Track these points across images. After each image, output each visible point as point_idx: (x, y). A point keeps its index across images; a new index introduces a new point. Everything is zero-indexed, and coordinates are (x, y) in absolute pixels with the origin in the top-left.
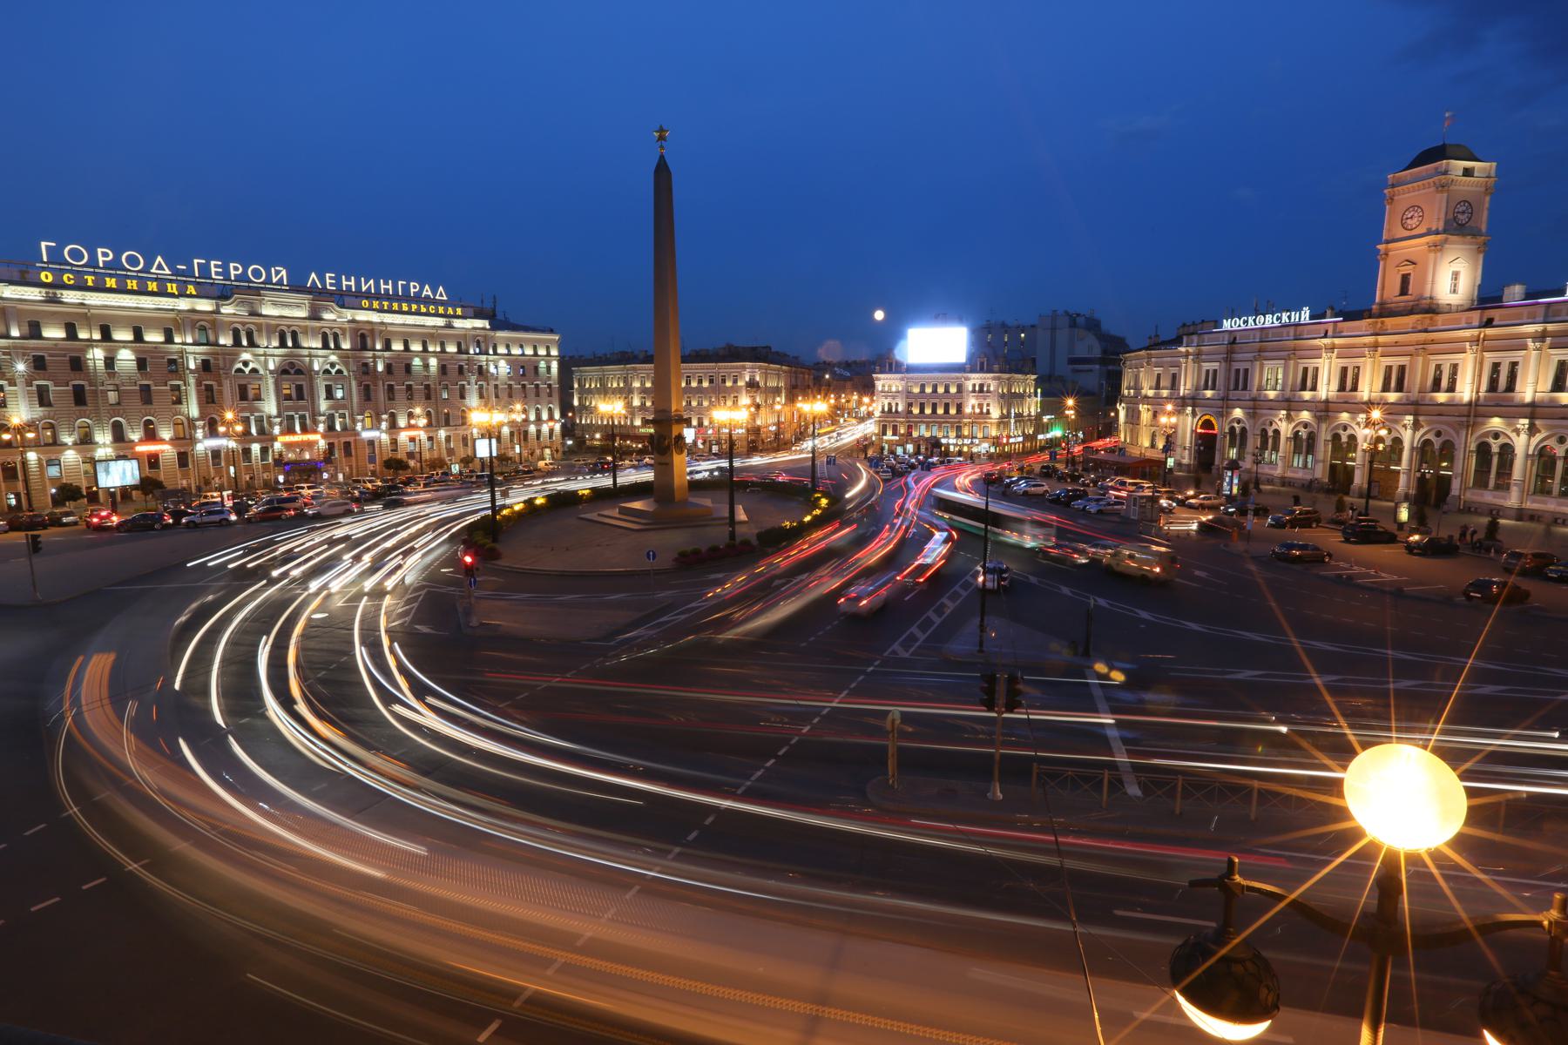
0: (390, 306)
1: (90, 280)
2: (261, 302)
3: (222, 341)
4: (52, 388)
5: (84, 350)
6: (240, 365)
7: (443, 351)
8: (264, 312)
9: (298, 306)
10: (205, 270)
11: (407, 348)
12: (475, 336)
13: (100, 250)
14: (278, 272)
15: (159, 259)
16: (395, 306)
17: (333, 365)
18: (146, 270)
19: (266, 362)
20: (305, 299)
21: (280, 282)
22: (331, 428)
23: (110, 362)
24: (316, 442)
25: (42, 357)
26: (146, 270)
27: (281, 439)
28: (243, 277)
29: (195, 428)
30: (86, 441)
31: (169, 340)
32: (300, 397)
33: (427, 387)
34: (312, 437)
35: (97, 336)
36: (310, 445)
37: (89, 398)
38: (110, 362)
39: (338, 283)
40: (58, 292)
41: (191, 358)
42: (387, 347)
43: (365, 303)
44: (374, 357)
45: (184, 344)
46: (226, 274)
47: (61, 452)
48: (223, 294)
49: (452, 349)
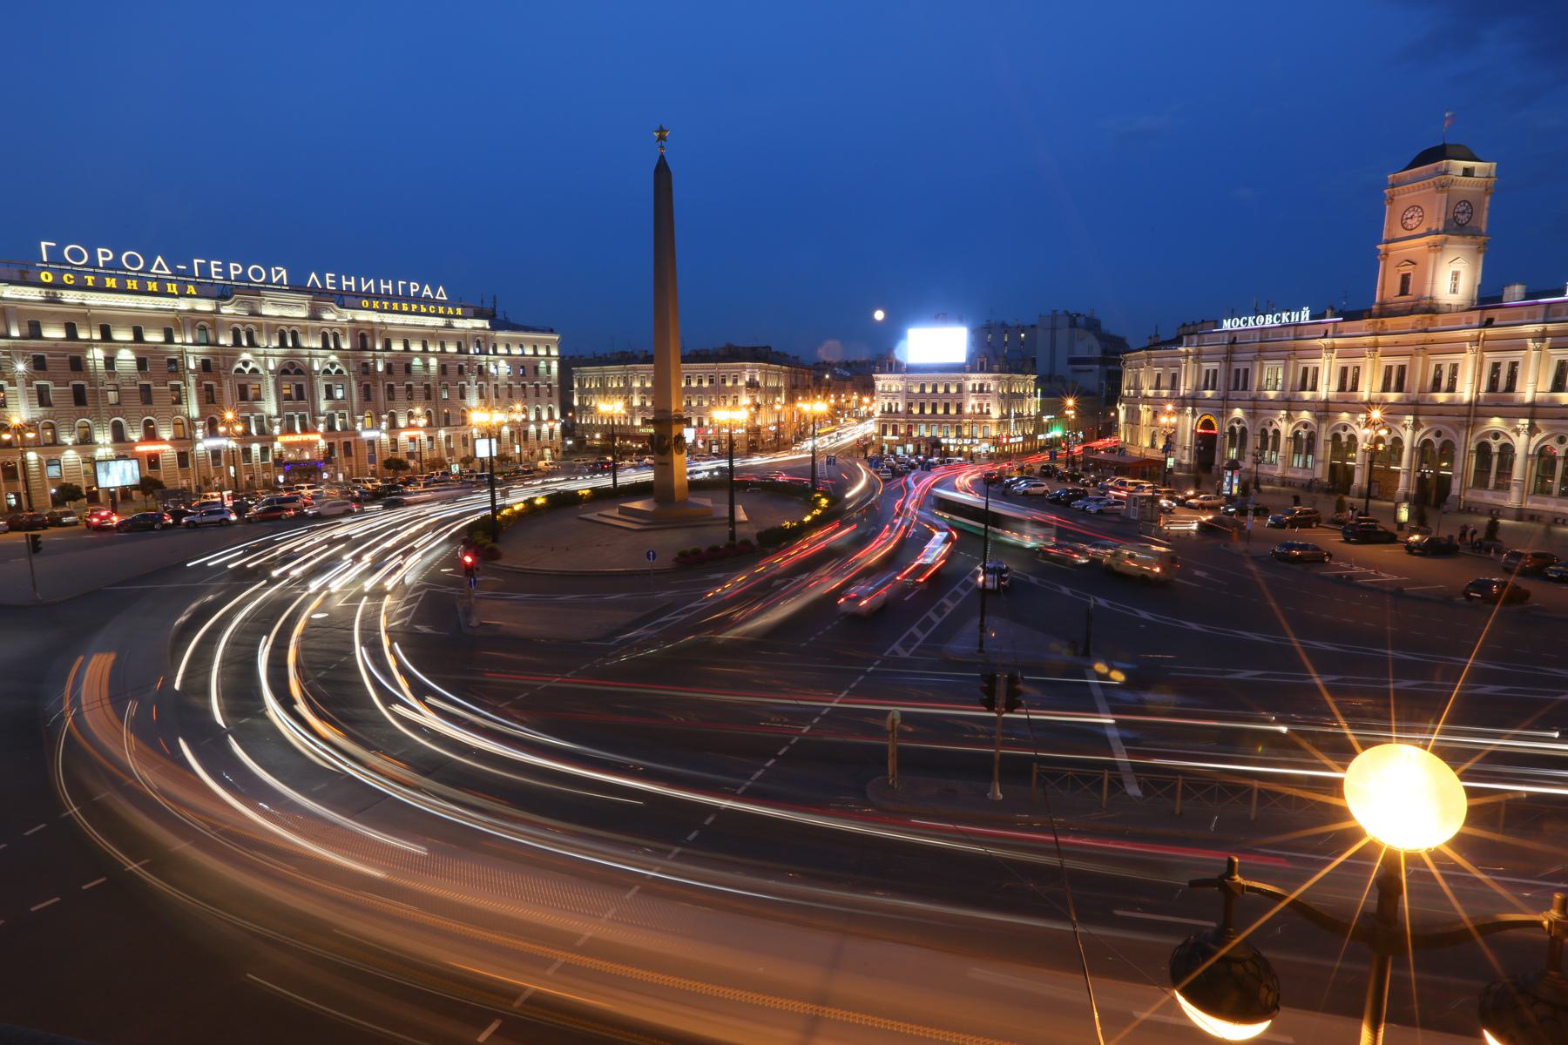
0: (390, 306)
1: (90, 280)
2: (261, 302)
3: (222, 341)
4: (52, 388)
5: (84, 350)
6: (240, 365)
7: (443, 351)
8: (264, 312)
9: (298, 306)
10: (205, 270)
11: (407, 348)
12: (475, 336)
13: (100, 250)
14: (278, 272)
15: (159, 259)
16: (395, 306)
17: (333, 365)
18: (146, 270)
19: (266, 362)
20: (305, 299)
21: (280, 282)
22: (331, 428)
23: (110, 362)
24: (316, 442)
25: (42, 357)
26: (146, 270)
27: (281, 439)
28: (243, 277)
29: (195, 428)
30: (86, 441)
31: (169, 340)
32: (300, 397)
33: (427, 387)
34: (312, 437)
35: (97, 336)
36: (310, 445)
37: (89, 398)
38: (110, 362)
39: (338, 283)
40: (58, 292)
41: (191, 358)
42: (387, 347)
43: (365, 303)
44: (374, 357)
45: (184, 344)
46: (226, 274)
47: (61, 452)
48: (223, 294)
49: (452, 349)
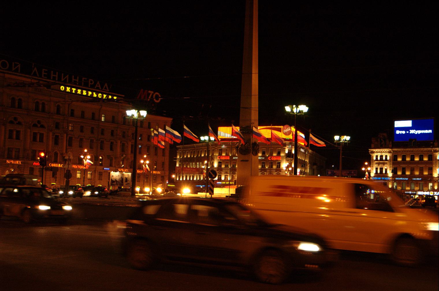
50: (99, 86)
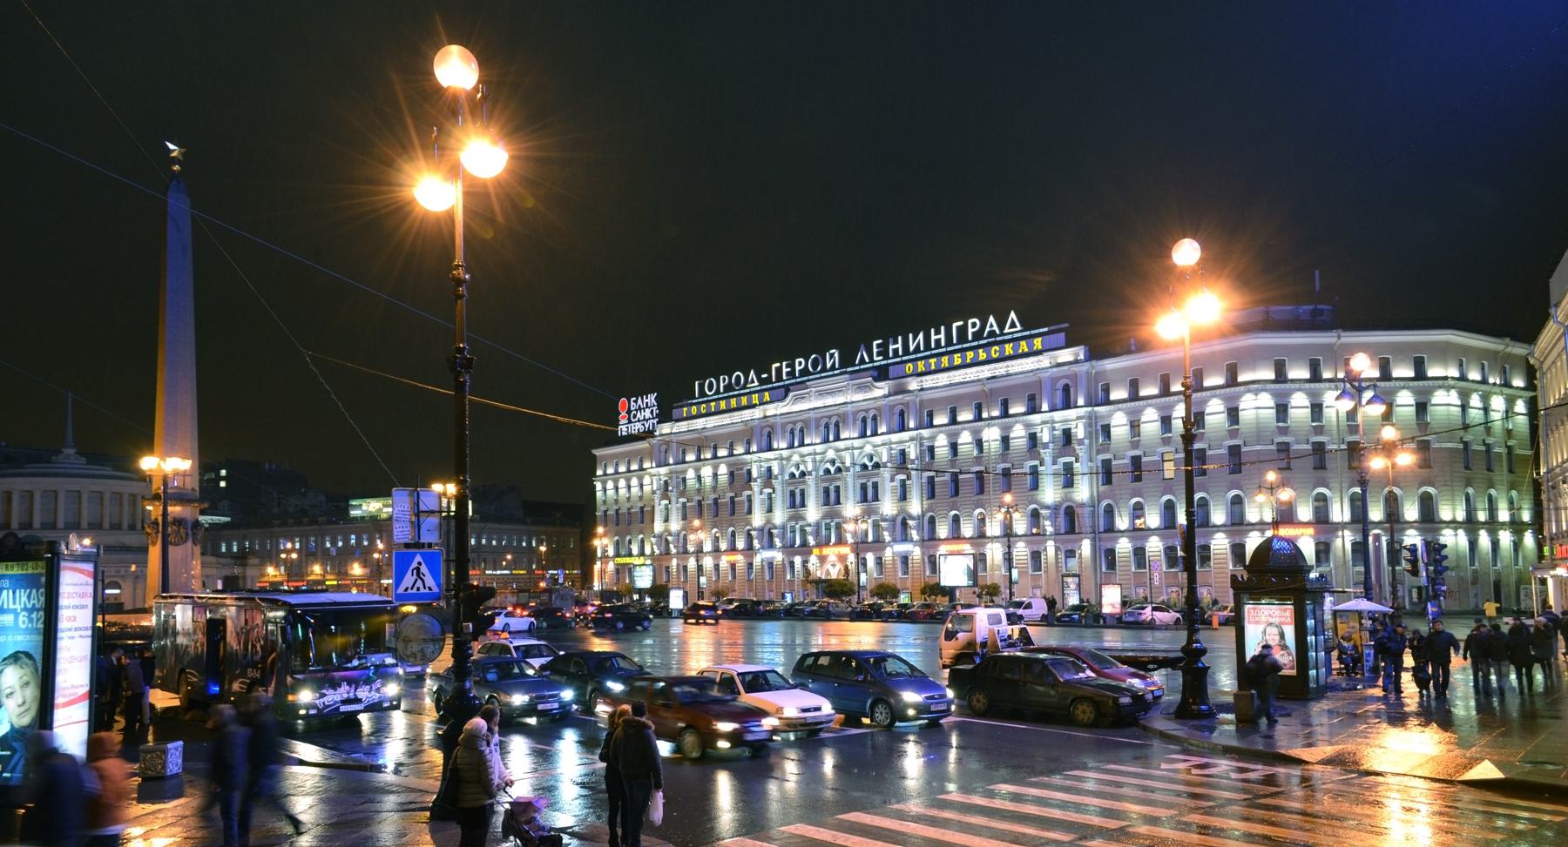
33: (1319, 449)
39: (884, 352)
50: (995, 328)
